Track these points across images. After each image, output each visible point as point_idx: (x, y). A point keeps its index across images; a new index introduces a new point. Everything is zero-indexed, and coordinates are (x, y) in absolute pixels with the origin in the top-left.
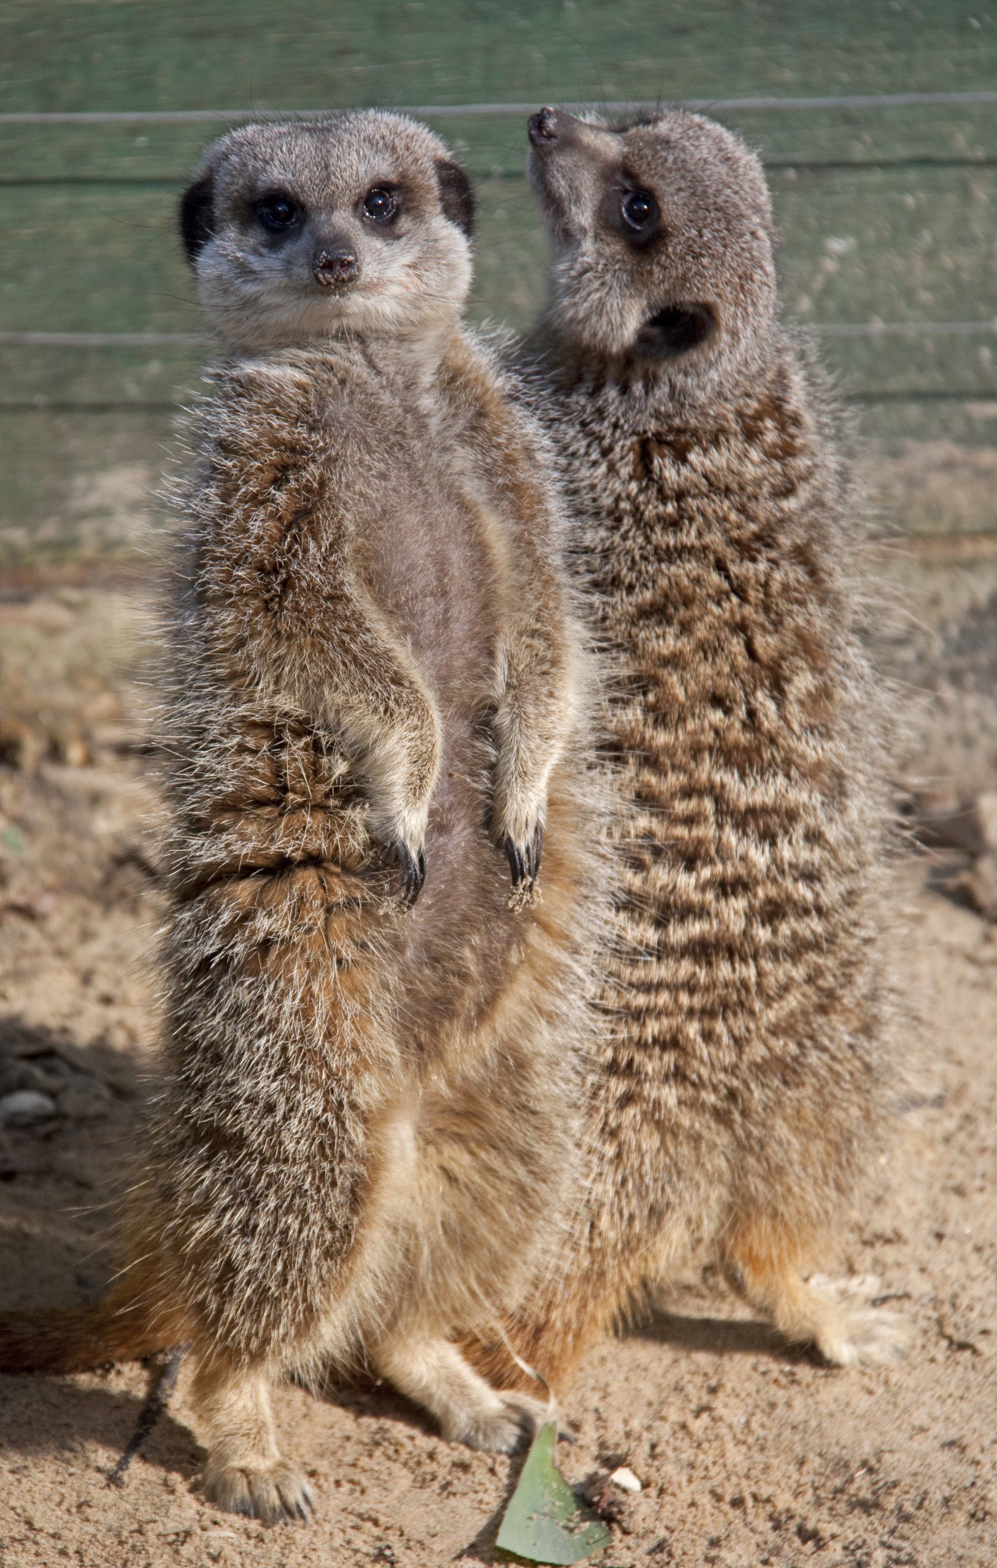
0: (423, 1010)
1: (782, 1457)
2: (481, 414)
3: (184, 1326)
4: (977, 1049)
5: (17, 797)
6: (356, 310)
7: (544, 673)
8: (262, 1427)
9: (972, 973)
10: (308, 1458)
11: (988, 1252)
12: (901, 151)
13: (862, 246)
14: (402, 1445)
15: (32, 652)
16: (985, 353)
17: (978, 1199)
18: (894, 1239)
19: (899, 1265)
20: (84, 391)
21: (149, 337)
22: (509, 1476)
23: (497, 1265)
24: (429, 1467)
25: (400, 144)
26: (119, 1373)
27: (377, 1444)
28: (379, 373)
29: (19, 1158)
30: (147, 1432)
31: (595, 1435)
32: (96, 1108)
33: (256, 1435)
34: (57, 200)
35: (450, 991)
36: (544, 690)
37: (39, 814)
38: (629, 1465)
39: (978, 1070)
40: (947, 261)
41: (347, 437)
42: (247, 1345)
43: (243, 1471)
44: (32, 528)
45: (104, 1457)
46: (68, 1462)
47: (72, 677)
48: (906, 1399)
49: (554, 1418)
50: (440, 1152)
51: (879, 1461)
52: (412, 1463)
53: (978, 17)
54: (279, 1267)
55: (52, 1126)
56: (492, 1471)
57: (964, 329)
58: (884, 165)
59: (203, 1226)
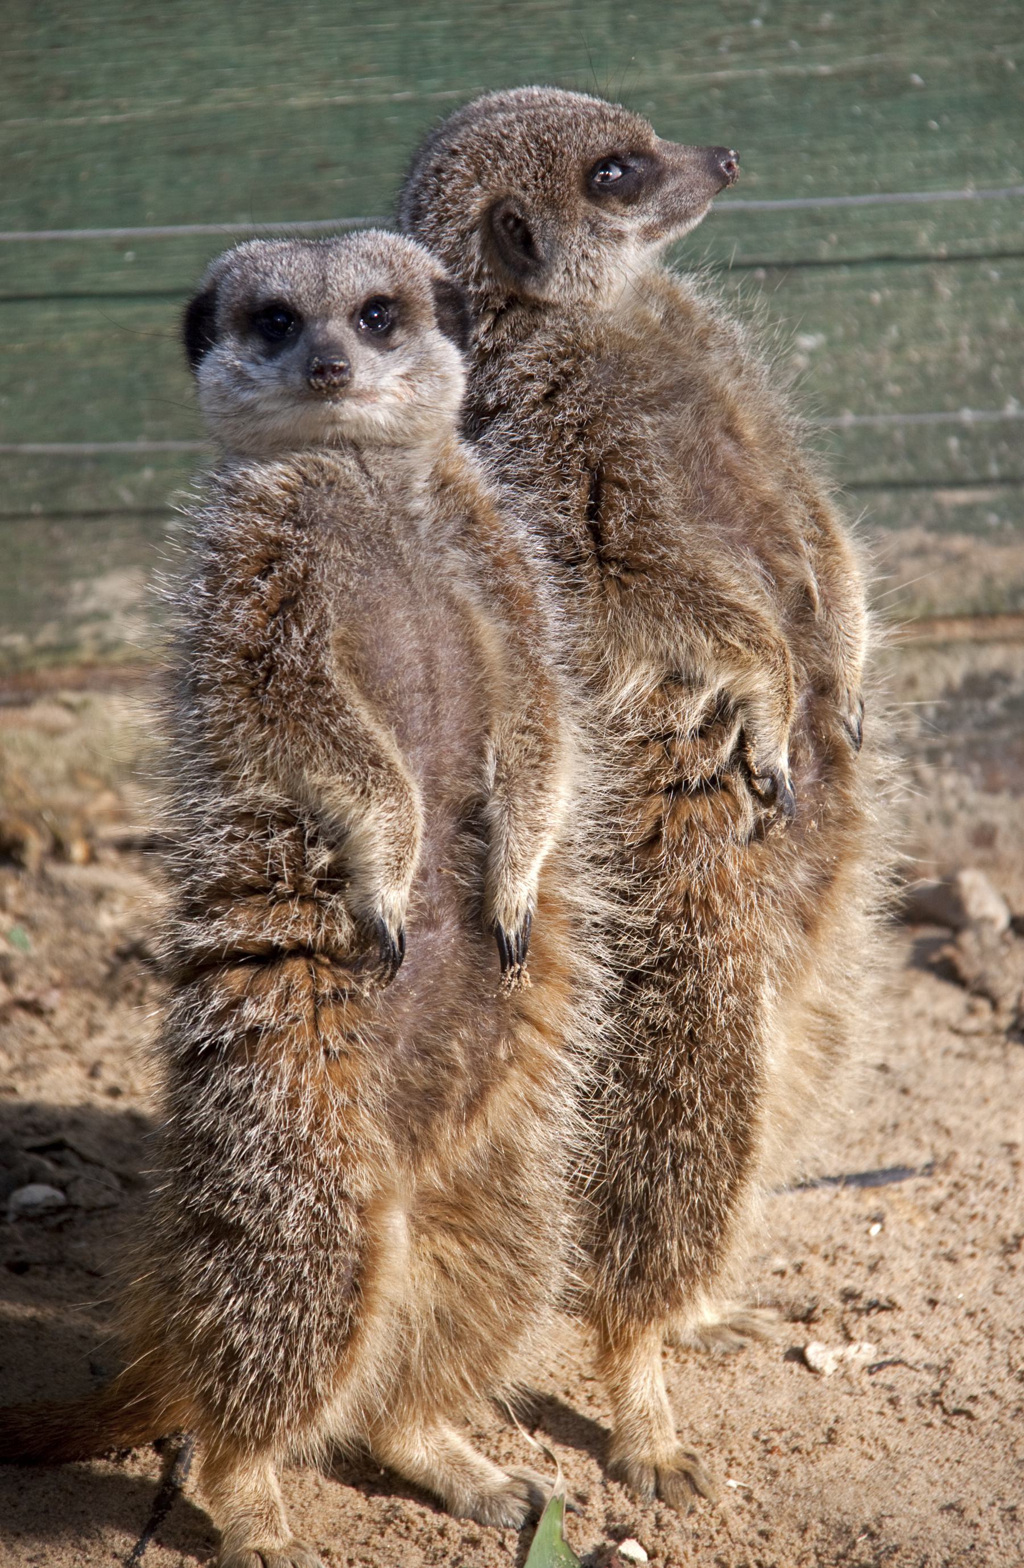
0: (415, 1101)
1: (785, 1524)
2: (472, 519)
3: (188, 1415)
4: (964, 1118)
5: (21, 895)
6: (349, 417)
7: (535, 767)
8: (273, 1507)
9: (957, 1044)
10: (320, 1538)
11: (980, 1317)
12: (866, 249)
13: (831, 343)
14: (413, 1523)
15: (34, 754)
16: (954, 443)
17: (970, 1265)
18: (890, 1306)
19: (894, 1331)
20: (79, 499)
21: (141, 445)
22: (518, 1551)
23: (489, 1357)
24: (439, 1544)
25: (397, 263)
26: (135, 1458)
27: (389, 1522)
28: (369, 476)
29: (31, 1250)
30: (162, 1517)
31: (602, 1507)
32: (110, 1197)
33: (268, 1515)
34: (50, 314)
35: (440, 1083)
36: (533, 782)
37: (44, 912)
38: (635, 1537)
39: (967, 1138)
40: (914, 354)
41: (331, 536)
42: (253, 1431)
43: (259, 1552)
44: (31, 635)
45: (122, 1541)
46: (84, 1549)
47: (73, 776)
48: (904, 1463)
49: (562, 1491)
50: (432, 1240)
51: (880, 1526)
52: (422, 1540)
53: (937, 119)
54: (281, 1354)
55: (62, 1217)
56: (502, 1546)
57: (932, 419)
58: (851, 263)
59: (206, 1317)
